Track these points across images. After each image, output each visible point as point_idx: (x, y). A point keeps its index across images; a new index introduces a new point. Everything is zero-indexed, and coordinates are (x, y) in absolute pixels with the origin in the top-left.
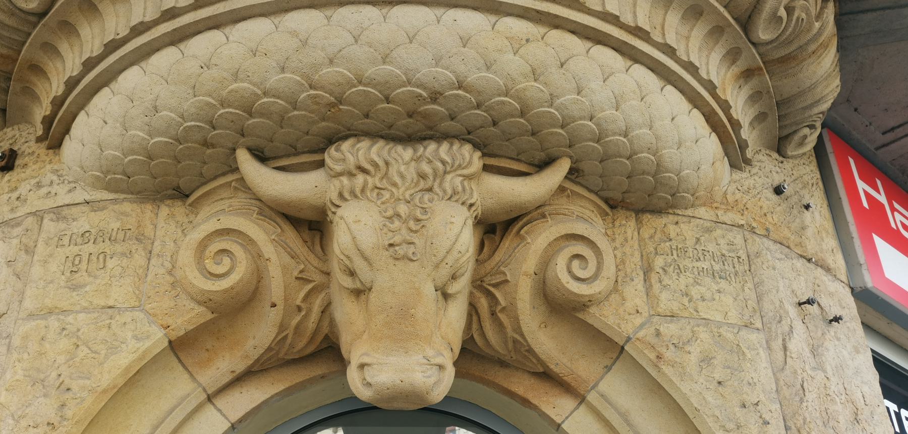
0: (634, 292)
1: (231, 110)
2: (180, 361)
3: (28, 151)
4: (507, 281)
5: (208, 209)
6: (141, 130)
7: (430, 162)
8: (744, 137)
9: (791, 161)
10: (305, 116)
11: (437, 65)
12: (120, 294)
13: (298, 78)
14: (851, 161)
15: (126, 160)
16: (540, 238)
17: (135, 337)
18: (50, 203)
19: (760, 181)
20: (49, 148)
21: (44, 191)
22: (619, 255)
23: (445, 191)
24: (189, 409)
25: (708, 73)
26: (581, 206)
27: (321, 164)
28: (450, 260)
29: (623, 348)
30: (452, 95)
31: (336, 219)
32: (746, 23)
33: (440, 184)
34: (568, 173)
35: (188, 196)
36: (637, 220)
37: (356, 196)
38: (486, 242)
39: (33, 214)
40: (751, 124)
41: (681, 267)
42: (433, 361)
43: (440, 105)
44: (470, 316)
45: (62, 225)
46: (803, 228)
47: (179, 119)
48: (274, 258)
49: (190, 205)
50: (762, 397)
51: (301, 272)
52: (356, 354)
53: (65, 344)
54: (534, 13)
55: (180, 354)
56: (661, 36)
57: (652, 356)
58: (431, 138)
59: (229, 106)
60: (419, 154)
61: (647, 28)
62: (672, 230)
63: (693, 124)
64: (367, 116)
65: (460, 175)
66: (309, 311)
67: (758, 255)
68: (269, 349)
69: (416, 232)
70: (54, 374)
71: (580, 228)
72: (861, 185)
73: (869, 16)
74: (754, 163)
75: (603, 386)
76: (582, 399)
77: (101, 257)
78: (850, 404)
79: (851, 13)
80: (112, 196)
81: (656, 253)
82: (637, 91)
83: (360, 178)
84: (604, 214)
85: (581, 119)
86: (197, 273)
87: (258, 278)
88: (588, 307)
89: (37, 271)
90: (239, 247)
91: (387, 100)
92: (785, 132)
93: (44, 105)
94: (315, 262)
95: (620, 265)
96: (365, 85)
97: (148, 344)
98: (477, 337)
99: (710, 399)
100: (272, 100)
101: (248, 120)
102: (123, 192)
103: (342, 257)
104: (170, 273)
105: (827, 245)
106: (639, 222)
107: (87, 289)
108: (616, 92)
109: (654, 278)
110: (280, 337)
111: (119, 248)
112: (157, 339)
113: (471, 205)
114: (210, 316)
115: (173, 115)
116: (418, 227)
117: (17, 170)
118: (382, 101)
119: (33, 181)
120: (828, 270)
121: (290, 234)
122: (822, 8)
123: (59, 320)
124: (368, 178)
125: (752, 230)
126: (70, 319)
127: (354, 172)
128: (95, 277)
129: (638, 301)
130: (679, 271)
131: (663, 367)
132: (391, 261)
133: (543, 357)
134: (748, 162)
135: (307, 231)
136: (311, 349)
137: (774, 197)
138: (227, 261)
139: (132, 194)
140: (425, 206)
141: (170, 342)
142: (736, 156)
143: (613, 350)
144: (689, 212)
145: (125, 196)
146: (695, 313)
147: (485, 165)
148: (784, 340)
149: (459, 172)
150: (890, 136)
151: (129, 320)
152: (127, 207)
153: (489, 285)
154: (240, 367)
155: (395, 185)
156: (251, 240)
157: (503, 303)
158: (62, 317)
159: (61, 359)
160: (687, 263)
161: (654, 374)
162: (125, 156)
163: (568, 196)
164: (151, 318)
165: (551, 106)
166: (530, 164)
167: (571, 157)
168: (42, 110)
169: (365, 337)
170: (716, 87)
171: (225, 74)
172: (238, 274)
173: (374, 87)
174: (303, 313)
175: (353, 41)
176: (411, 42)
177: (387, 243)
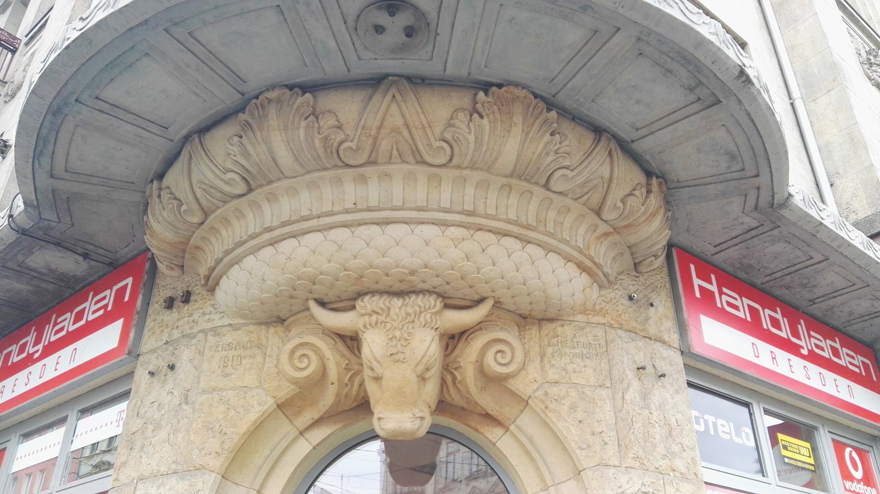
0: (533, 371)
3: (197, 292)
4: (460, 367)
7: (413, 307)
12: (250, 379)
14: (692, 267)
16: (478, 343)
17: (259, 404)
18: (210, 325)
19: (619, 293)
20: (208, 291)
21: (207, 317)
24: (290, 440)
27: (353, 308)
28: (424, 361)
39: (202, 331)
42: (417, 415)
44: (442, 385)
45: (217, 339)
46: (647, 320)
52: (378, 410)
55: (285, 411)
57: (543, 407)
64: (377, 283)
66: (352, 385)
67: (612, 341)
68: (332, 406)
70: (217, 425)
72: (697, 282)
73: (687, 189)
75: (518, 422)
79: (676, 188)
83: (374, 317)
89: (206, 365)
91: (387, 275)
95: (526, 354)
97: (265, 408)
99: (574, 431)
104: (276, 366)
105: (667, 328)
109: (546, 360)
111: (248, 352)
112: (270, 403)
114: (298, 390)
117: (192, 303)
119: (201, 311)
120: (664, 342)
121: (340, 345)
122: (646, 197)
124: (379, 317)
125: (611, 326)
126: (224, 394)
129: (536, 375)
136: (355, 404)
137: (627, 303)
138: (306, 360)
141: (278, 405)
150: (718, 249)
154: (316, 416)
155: (393, 320)
157: (459, 378)
159: (221, 417)
160: (567, 350)
161: (543, 416)
169: (381, 402)
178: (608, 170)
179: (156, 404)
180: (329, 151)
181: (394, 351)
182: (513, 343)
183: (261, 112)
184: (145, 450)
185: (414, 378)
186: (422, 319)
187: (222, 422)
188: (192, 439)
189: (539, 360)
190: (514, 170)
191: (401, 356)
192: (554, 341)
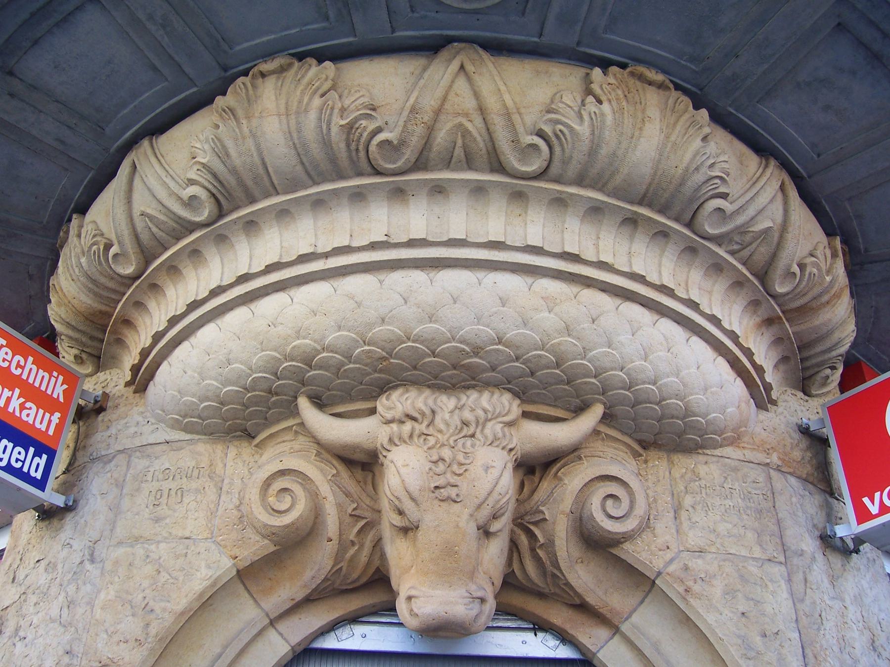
1: (294, 363)
2: (246, 588)
4: (545, 520)
5: (272, 450)
6: (216, 380)
7: (473, 410)
8: (768, 380)
9: (815, 399)
10: (359, 368)
11: (478, 324)
13: (354, 336)
15: (202, 405)
16: (574, 479)
17: (208, 567)
20: (135, 392)
22: (651, 494)
23: (486, 437)
25: (730, 324)
26: (615, 448)
27: (373, 411)
28: (491, 501)
29: (654, 582)
30: (491, 350)
31: (386, 462)
32: (763, 276)
33: (482, 430)
34: (602, 418)
35: (253, 438)
36: (668, 461)
37: (405, 442)
38: (526, 483)
40: (775, 366)
41: (709, 505)
43: (481, 358)
47: (249, 371)
48: (331, 498)
49: (256, 446)
50: (782, 627)
51: (355, 509)
53: (149, 569)
54: (567, 275)
55: (246, 582)
56: (685, 292)
57: (681, 589)
58: (473, 387)
59: (292, 360)
60: (462, 403)
61: (672, 286)
62: (702, 470)
63: (722, 369)
64: (415, 368)
65: (501, 422)
66: (362, 546)
68: (326, 579)
69: (460, 475)
70: (140, 596)
71: (613, 470)
74: (780, 404)
75: (635, 618)
76: (616, 630)
77: (179, 492)
78: (867, 631)
80: (188, 437)
81: (687, 492)
82: (664, 342)
83: (408, 427)
84: (636, 455)
85: (612, 370)
86: (261, 509)
87: (317, 514)
88: (622, 543)
90: (299, 486)
92: (808, 373)
93: (133, 354)
94: (368, 501)
96: (414, 342)
98: (518, 573)
100: (330, 354)
101: (309, 372)
102: (198, 433)
103: (392, 498)
106: (671, 462)
107: (167, 521)
108: (645, 344)
109: (684, 515)
110: (335, 569)
111: (194, 485)
113: (511, 450)
114: (272, 548)
115: (243, 367)
116: (461, 471)
118: (429, 356)
123: (144, 548)
124: (416, 425)
126: (153, 547)
127: (403, 419)
128: (175, 511)
130: (707, 508)
131: (691, 600)
132: (436, 502)
133: (579, 590)
134: (774, 403)
135: (360, 472)
138: (288, 499)
139: (205, 435)
140: (467, 451)
141: (238, 571)
142: (762, 398)
143: (642, 582)
144: (717, 452)
145: (199, 437)
146: (722, 548)
147: (524, 412)
148: (804, 572)
149: (500, 419)
151: (203, 549)
152: (201, 447)
153: (529, 523)
154: (300, 596)
155: (440, 431)
156: (310, 479)
158: (146, 546)
159: (146, 583)
162: (202, 402)
163: (603, 439)
164: (221, 549)
165: (584, 358)
166: (567, 410)
167: (604, 404)
168: (130, 359)
169: (413, 571)
170: (739, 337)
171: (289, 332)
172: (297, 511)
173: (422, 343)
174: (356, 548)
175: (403, 301)
176: (455, 302)
177: (433, 485)
178: (780, 212)
179: (43, 564)
180: (353, 147)
181: (441, 481)
182: (631, 484)
183: (251, 92)
184: (22, 634)
185: (472, 529)
186: (488, 431)
187: (147, 591)
188: (98, 616)
189: (672, 514)
190: (644, 196)
191: (453, 492)
192: (695, 485)
